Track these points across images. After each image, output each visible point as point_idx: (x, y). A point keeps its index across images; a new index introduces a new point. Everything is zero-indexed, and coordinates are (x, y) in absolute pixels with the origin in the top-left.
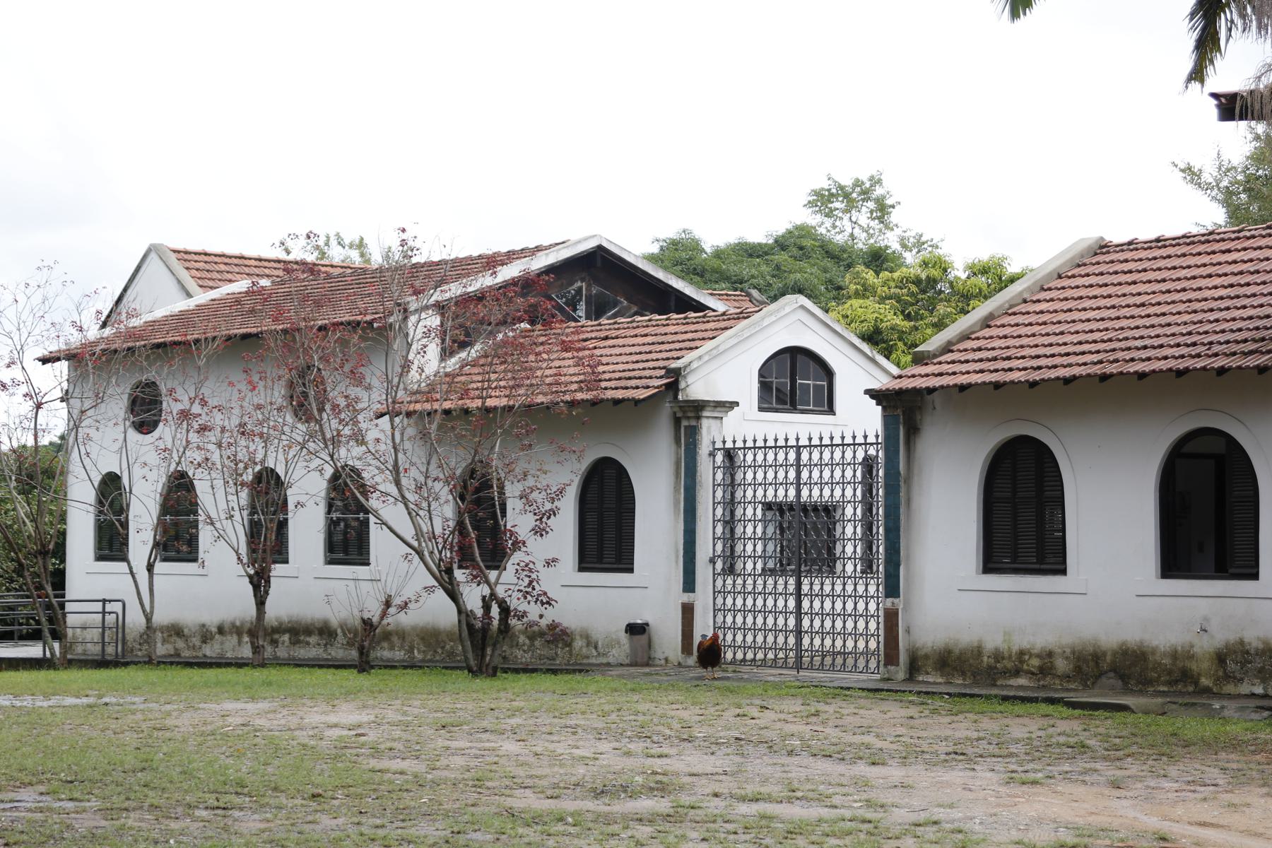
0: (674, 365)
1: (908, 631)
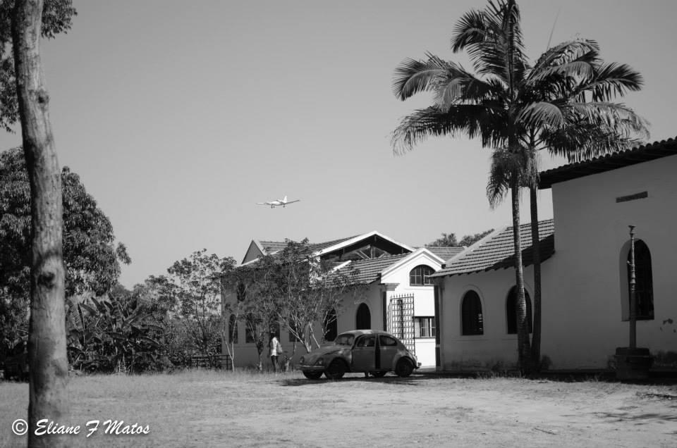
0: (379, 272)
1: (443, 355)
